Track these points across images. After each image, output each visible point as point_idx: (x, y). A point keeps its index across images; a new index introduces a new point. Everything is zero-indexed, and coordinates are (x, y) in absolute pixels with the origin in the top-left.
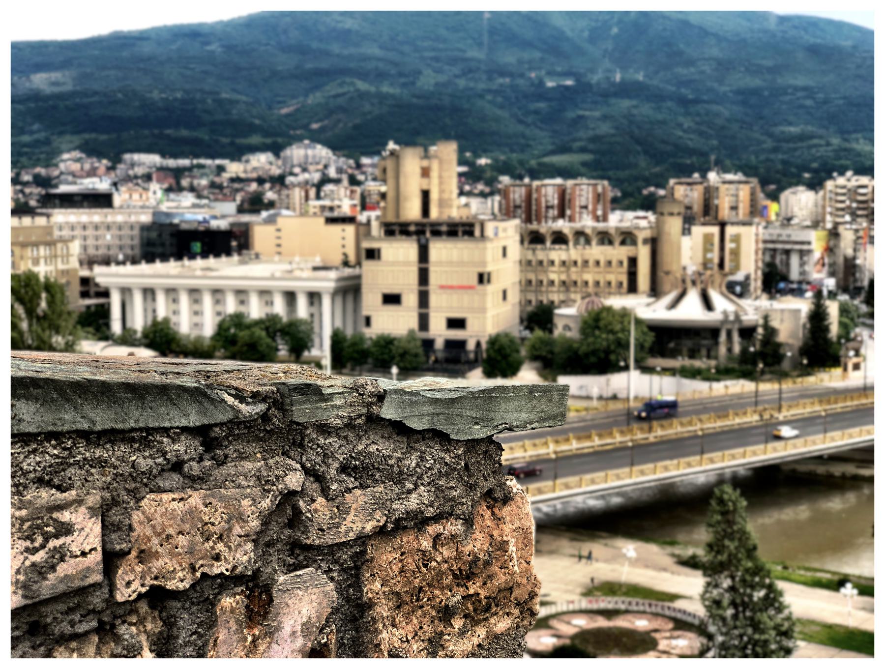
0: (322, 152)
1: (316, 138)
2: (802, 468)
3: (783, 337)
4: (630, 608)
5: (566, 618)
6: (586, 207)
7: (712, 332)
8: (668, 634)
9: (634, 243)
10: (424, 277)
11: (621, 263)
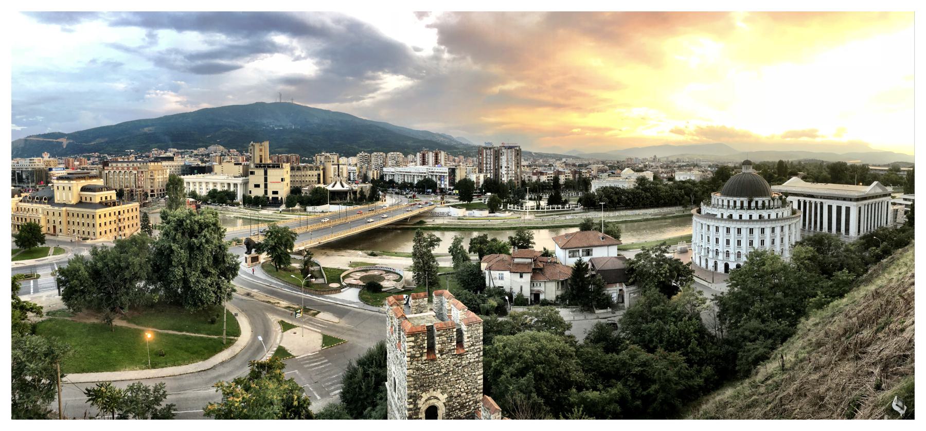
0: (221, 148)
1: (219, 144)
10: (266, 180)
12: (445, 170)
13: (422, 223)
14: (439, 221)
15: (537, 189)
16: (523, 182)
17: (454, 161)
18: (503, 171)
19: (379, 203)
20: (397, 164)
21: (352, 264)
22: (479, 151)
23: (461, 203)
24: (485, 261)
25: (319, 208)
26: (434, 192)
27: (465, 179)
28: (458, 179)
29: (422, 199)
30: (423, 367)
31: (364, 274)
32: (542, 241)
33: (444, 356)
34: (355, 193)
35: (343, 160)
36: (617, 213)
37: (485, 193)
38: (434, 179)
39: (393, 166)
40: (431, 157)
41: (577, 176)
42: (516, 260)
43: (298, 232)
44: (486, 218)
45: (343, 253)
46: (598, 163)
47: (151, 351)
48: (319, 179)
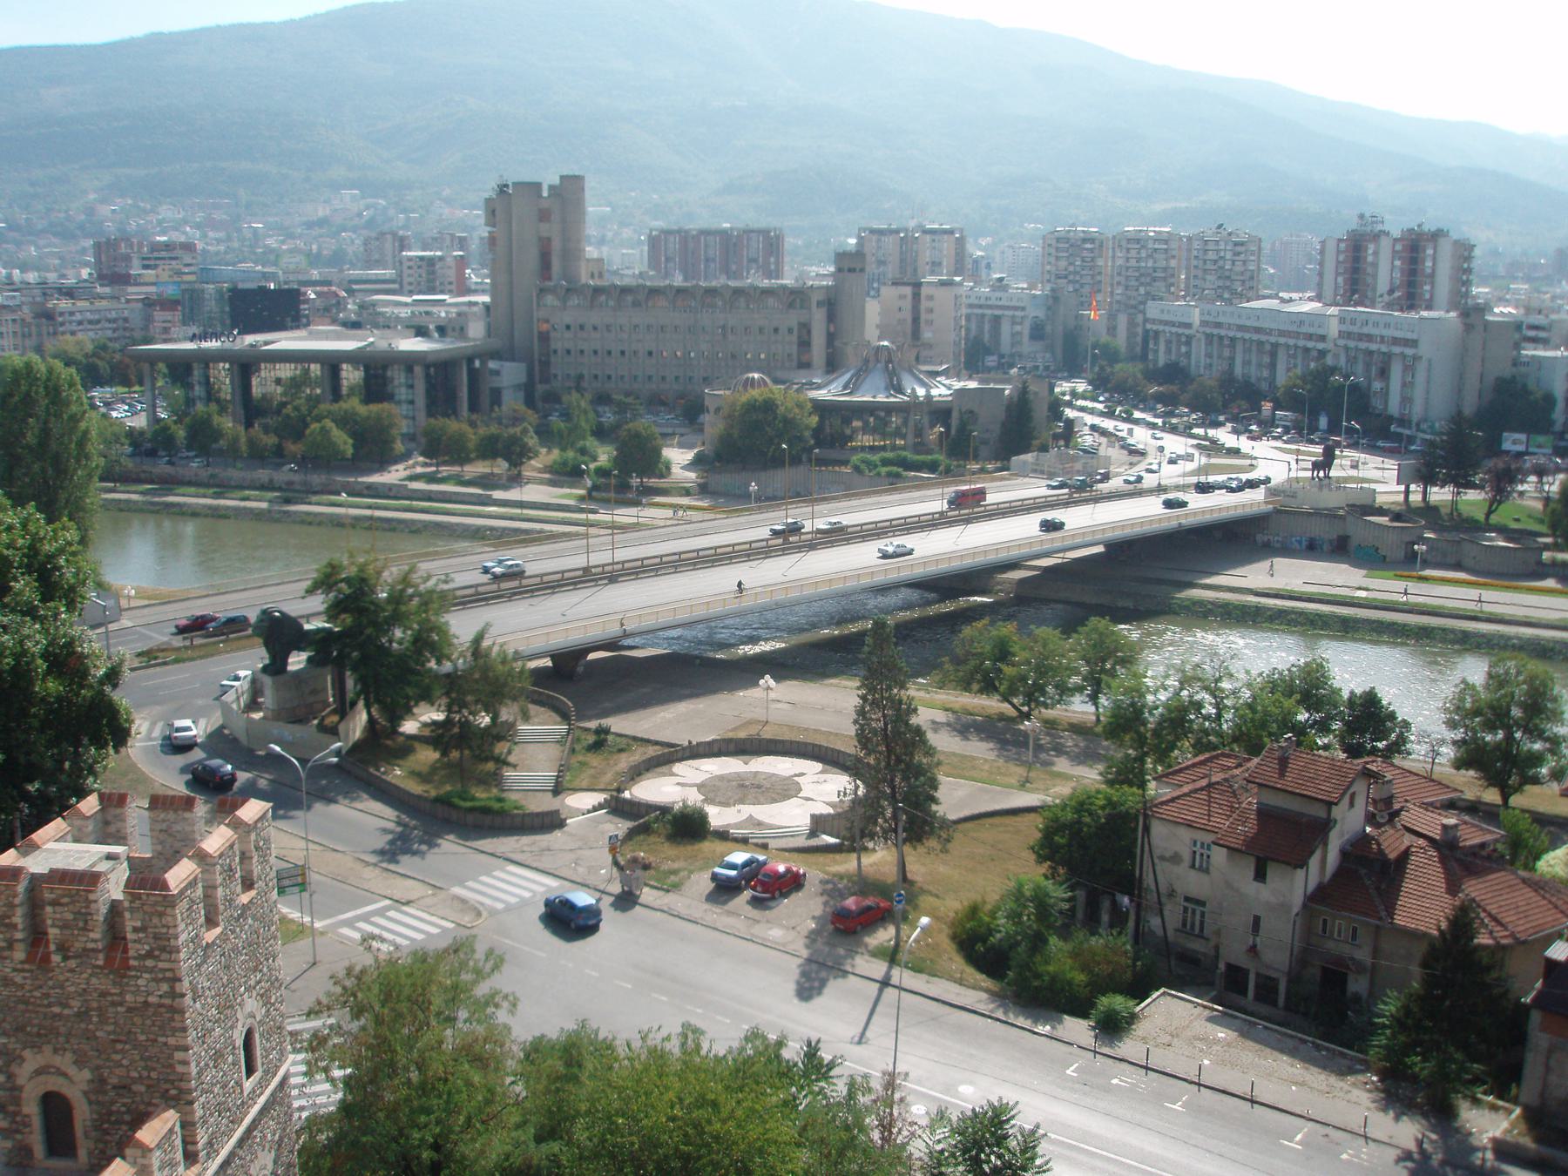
6: (755, 260)
8: (816, 778)
23: (1373, 486)
30: (18, 979)
33: (72, 963)
47: (1110, 783)
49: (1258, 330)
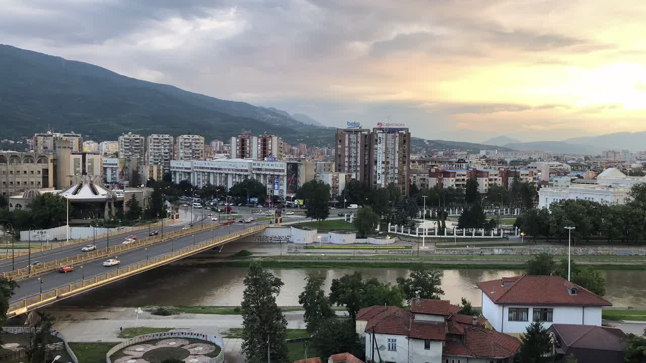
2: (181, 263)
3: (141, 205)
4: (161, 337)
5: (129, 348)
7: (101, 204)
9: (46, 162)
11: (39, 172)
12: (281, 166)
13: (244, 254)
14: (273, 252)
15: (440, 201)
16: (413, 188)
17: (291, 152)
18: (379, 169)
19: (167, 221)
20: (195, 155)
21: (124, 333)
22: (337, 136)
23: (309, 220)
24: (361, 319)
25: (51, 233)
26: (262, 202)
27: (314, 182)
28: (302, 181)
29: (240, 213)
31: (151, 347)
32: (453, 289)
34: (119, 204)
35: (89, 146)
36: (591, 251)
37: (348, 204)
38: (262, 181)
39: (187, 158)
40: (255, 145)
41: (511, 180)
42: (419, 318)
43: (15, 278)
44: (354, 246)
45: (105, 314)
46: (549, 158)
48: (45, 178)
49: (219, 169)
